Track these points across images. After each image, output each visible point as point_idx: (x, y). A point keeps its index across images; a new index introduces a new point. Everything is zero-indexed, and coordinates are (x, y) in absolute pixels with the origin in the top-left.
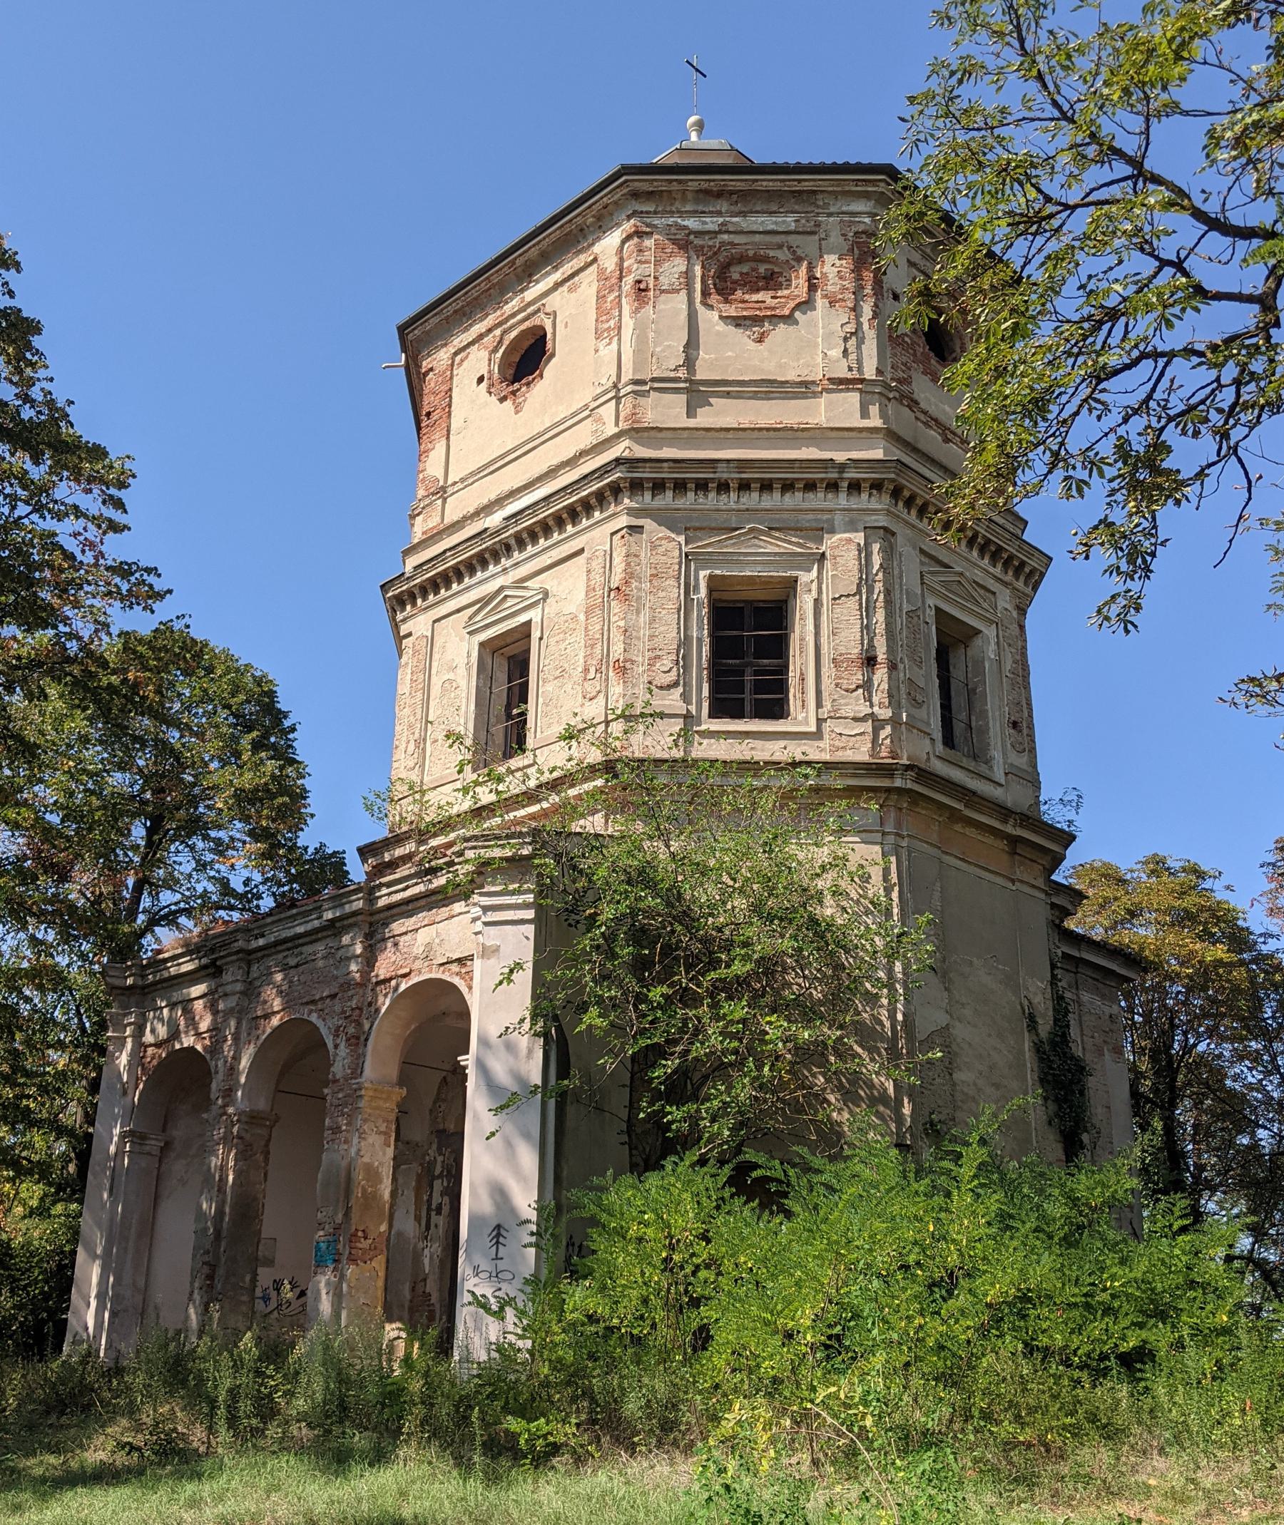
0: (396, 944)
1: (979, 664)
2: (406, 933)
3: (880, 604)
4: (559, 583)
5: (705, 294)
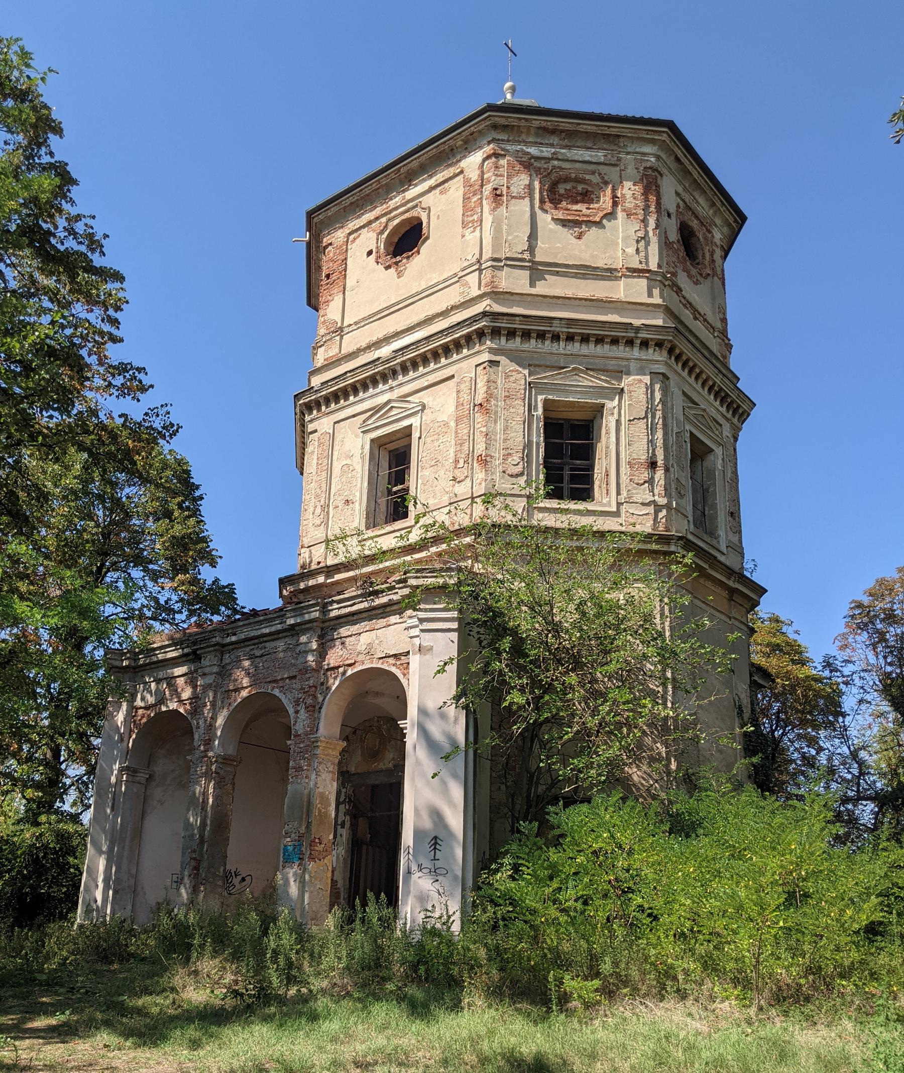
0: (343, 643)
1: (711, 473)
2: (351, 636)
3: (660, 426)
4: (434, 399)
5: (542, 202)
